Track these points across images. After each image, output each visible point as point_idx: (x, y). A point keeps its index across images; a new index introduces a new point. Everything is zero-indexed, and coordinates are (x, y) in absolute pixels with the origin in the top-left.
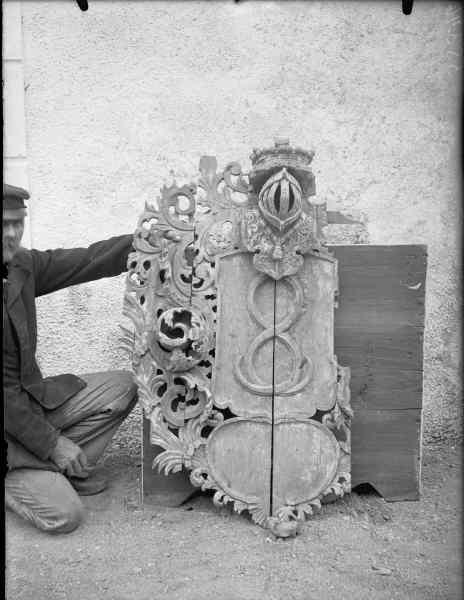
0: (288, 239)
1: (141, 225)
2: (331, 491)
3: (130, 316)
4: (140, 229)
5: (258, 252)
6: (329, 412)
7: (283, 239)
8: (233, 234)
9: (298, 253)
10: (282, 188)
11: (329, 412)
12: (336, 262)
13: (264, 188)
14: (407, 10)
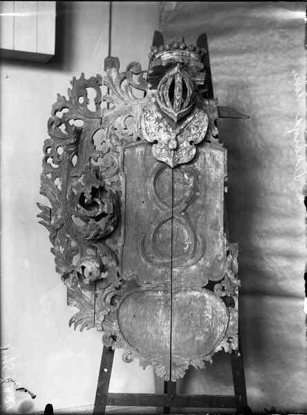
0: (182, 131)
1: (55, 114)
2: (221, 349)
3: (46, 195)
4: (54, 118)
5: (156, 142)
6: (220, 282)
7: (178, 131)
8: (201, 344)
9: (191, 143)
10: (176, 81)
11: (220, 282)
12: (226, 151)
13: (161, 82)
14: (49, 407)
